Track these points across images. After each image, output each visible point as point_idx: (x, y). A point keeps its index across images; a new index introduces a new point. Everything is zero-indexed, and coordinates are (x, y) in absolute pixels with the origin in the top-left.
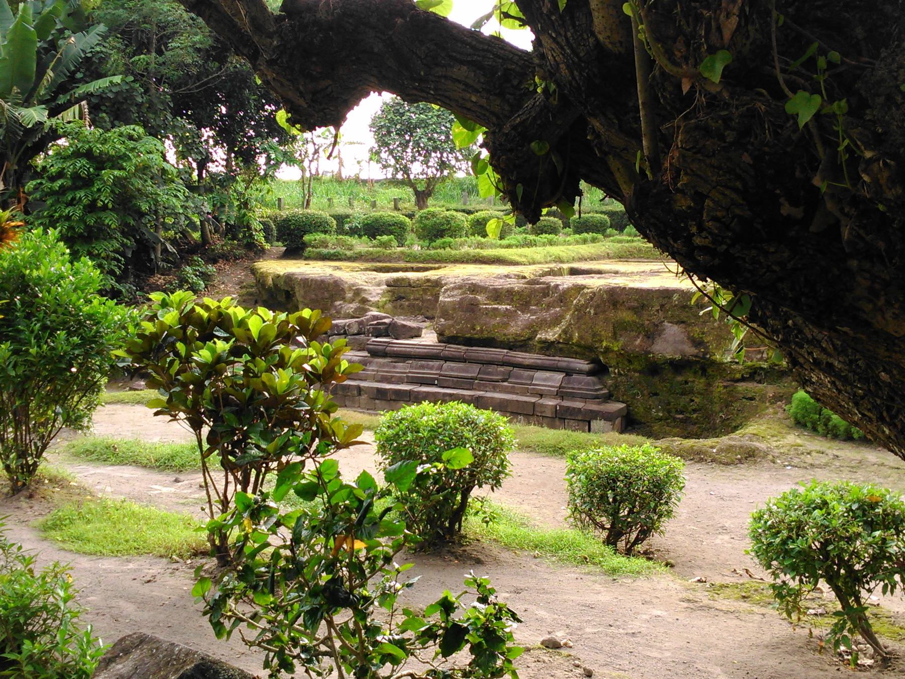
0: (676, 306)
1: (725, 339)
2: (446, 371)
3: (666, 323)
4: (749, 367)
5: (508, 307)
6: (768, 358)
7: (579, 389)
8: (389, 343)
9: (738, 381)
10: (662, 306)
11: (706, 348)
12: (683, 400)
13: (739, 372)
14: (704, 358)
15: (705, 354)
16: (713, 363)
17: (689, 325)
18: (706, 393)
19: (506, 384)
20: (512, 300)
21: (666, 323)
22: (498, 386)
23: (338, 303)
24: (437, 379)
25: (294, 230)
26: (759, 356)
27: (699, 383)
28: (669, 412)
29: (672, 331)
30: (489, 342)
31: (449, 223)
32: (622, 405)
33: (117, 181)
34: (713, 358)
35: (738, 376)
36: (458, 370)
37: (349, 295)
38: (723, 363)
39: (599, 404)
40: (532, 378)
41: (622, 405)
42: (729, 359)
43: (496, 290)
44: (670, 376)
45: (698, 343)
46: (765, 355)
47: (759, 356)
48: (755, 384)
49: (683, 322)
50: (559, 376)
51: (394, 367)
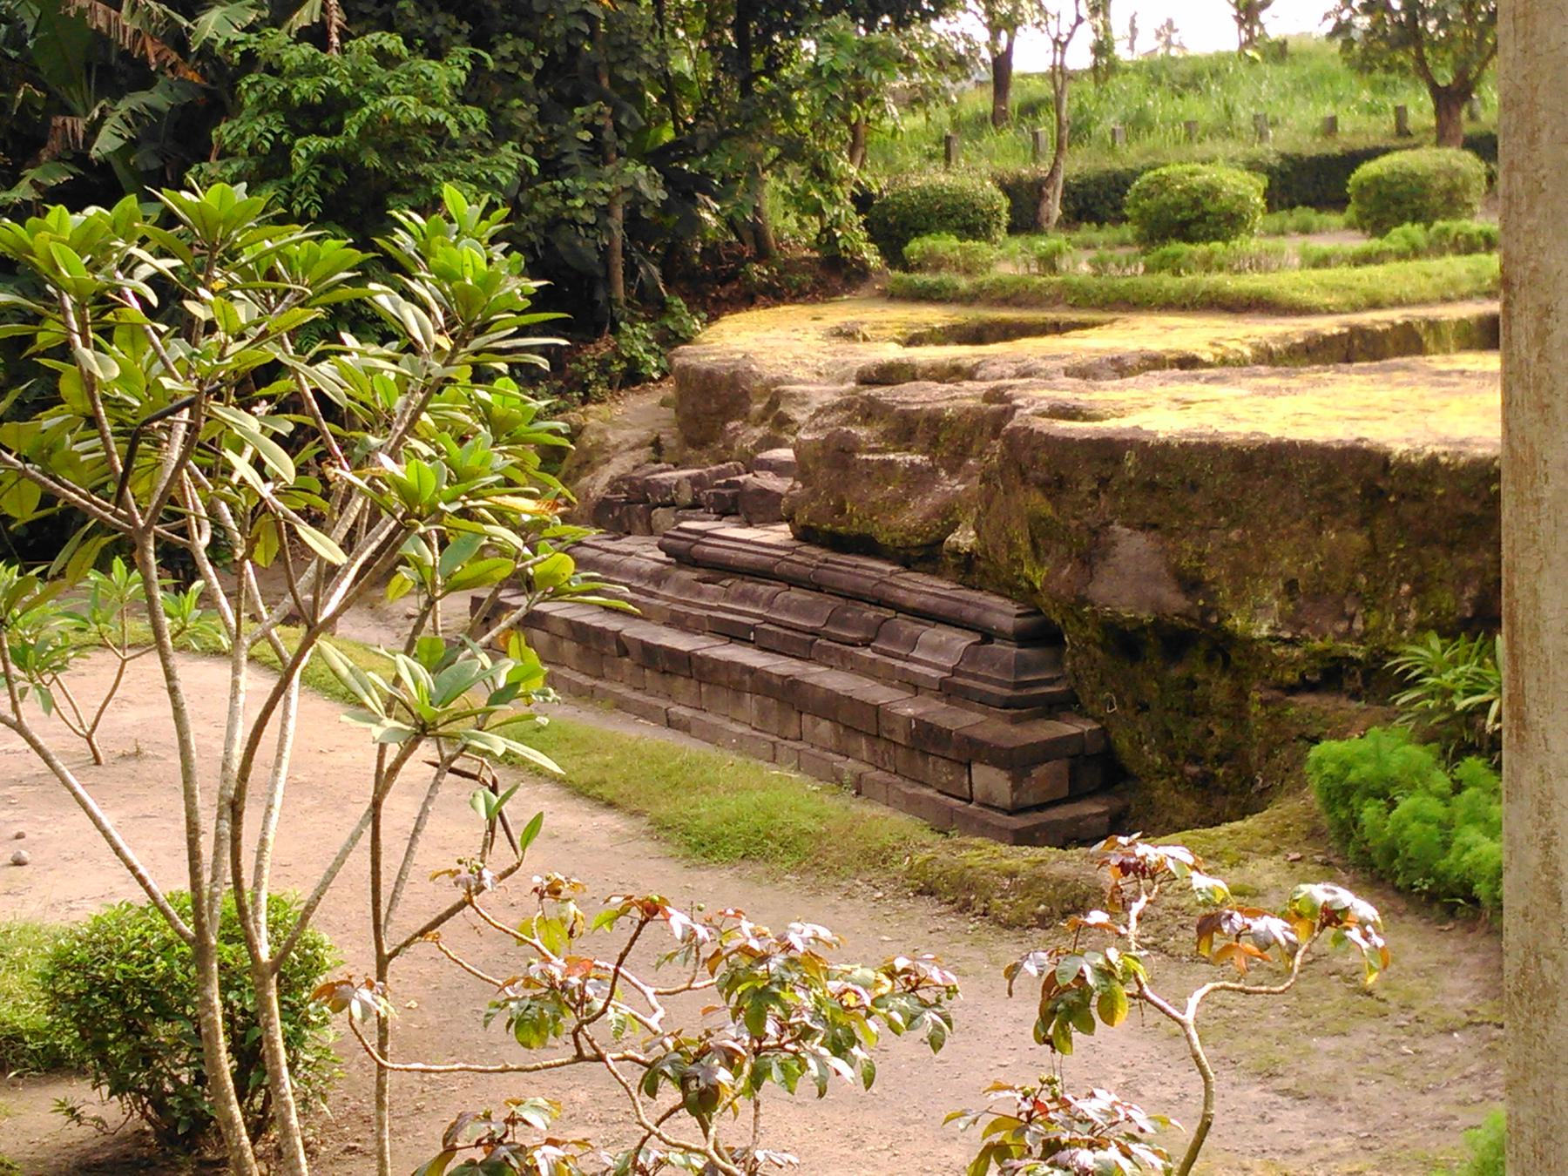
0: (1131, 482)
1: (1255, 576)
2: (777, 610)
3: (1117, 527)
4: (1315, 655)
5: (918, 459)
6: (1366, 634)
7: (988, 680)
8: (704, 534)
9: (1292, 690)
10: (1103, 482)
11: (1210, 596)
12: (1195, 728)
13: (1294, 664)
14: (1204, 623)
15: (1206, 612)
16: (1230, 638)
17: (1171, 532)
18: (1237, 715)
19: (868, 653)
20: (935, 442)
21: (1117, 527)
22: (844, 657)
23: (731, 425)
24: (753, 628)
25: (894, 226)
26: (1342, 627)
27: (1219, 690)
28: (1173, 756)
29: (1131, 545)
30: (867, 546)
31: (1196, 203)
32: (1087, 726)
33: (325, 160)
34: (1229, 623)
35: (1290, 677)
36: (802, 610)
37: (757, 407)
38: (1253, 640)
39: (1015, 721)
40: (913, 642)
41: (1087, 726)
42: (1265, 632)
43: (905, 415)
44: (1157, 663)
45: (1190, 584)
46: (1358, 625)
47: (1342, 627)
48: (1343, 702)
49: (1155, 526)
50: (961, 641)
51: (700, 594)
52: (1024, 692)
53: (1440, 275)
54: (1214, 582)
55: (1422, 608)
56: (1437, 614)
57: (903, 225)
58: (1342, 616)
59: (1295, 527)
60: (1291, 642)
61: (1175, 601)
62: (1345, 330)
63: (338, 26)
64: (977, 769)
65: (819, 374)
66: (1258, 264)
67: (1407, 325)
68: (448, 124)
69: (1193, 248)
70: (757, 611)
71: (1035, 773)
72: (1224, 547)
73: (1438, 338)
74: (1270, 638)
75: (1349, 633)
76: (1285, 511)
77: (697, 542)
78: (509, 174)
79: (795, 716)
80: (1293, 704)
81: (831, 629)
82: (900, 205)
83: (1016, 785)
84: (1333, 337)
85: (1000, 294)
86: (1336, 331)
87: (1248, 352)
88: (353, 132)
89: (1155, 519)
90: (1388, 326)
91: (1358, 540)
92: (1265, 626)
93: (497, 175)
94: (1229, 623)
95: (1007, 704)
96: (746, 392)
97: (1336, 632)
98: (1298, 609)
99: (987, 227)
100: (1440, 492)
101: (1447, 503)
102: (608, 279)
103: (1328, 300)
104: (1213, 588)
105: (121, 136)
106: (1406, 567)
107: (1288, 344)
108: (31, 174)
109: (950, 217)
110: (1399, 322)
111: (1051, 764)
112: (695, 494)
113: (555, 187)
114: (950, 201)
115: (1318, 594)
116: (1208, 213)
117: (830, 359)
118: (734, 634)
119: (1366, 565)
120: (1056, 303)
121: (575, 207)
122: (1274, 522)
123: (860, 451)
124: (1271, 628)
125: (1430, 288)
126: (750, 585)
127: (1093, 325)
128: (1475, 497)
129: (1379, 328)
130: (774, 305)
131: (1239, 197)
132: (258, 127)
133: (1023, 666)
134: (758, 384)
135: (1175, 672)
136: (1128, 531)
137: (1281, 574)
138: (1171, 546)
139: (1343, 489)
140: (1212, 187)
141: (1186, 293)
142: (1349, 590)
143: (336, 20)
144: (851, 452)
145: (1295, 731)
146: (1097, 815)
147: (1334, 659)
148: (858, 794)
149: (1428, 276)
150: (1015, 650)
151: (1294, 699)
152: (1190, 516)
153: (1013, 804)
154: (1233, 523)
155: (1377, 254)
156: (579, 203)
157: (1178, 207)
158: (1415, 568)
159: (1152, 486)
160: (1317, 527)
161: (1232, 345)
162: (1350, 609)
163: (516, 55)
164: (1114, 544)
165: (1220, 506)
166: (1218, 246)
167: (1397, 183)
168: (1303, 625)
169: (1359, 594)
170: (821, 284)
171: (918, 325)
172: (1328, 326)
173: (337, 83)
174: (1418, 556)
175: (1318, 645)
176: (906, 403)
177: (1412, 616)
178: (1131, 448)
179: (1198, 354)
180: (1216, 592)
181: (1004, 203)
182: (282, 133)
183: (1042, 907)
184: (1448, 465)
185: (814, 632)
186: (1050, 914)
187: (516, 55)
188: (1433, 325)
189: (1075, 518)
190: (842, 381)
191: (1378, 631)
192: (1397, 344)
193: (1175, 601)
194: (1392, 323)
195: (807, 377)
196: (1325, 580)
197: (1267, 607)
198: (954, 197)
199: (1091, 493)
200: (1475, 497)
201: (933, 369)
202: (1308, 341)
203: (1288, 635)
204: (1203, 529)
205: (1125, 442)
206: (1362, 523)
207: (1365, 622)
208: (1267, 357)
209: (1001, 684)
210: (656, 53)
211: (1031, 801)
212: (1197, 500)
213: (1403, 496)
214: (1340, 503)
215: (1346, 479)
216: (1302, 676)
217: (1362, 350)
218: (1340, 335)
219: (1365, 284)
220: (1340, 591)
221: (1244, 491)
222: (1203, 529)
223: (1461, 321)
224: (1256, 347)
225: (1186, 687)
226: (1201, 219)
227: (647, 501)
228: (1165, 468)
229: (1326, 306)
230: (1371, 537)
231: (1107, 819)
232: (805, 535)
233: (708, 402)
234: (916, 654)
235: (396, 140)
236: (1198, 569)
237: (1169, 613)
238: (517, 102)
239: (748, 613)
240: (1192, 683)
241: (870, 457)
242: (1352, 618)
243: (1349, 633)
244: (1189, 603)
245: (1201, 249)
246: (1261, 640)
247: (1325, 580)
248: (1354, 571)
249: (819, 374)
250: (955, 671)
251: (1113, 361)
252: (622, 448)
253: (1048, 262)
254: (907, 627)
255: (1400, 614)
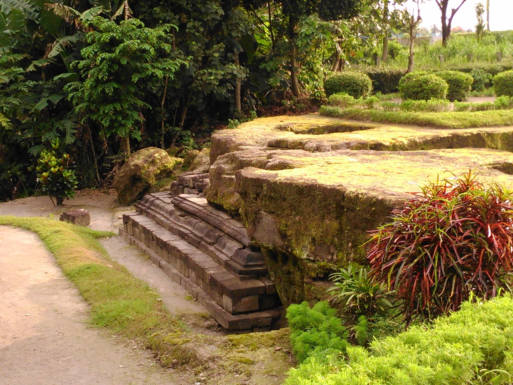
1: (303, 235)
4: (320, 267)
6: (337, 261)
10: (258, 195)
13: (314, 270)
15: (288, 247)
17: (278, 215)
21: (263, 212)
26: (330, 257)
31: (421, 86)
34: (294, 252)
35: (313, 274)
39: (242, 279)
45: (284, 236)
47: (330, 257)
51: (179, 220)
52: (248, 269)
53: (506, 116)
54: (290, 236)
55: (355, 252)
56: (360, 256)
57: (332, 89)
58: (329, 253)
59: (316, 217)
60: (313, 261)
61: (279, 242)
62: (450, 135)
63: (128, 16)
64: (224, 296)
65: (257, 142)
66: (433, 109)
67: (478, 134)
68: (151, 50)
69: (414, 102)
70: (190, 229)
71: (243, 300)
72: (294, 223)
73: (493, 140)
74: (307, 259)
75: (331, 260)
76: (313, 211)
77: (181, 202)
78: (177, 68)
79: (187, 268)
80: (314, 285)
81: (206, 238)
82: (331, 82)
83: (234, 303)
84: (444, 138)
85: (351, 115)
86: (446, 136)
87: (406, 142)
88: (117, 51)
89: (272, 210)
90: (470, 135)
91: (335, 224)
92: (306, 254)
93: (172, 68)
94: (294, 252)
95: (241, 273)
96: (228, 148)
97: (328, 259)
98: (316, 249)
99: (362, 91)
100: (358, 208)
101: (360, 213)
102: (235, 104)
103: (454, 124)
104: (290, 238)
105: (58, 51)
106: (350, 237)
107: (424, 140)
108: (35, 62)
109: (347, 87)
110: (475, 133)
111: (251, 297)
112: (194, 184)
113: (204, 72)
114: (347, 81)
115: (322, 244)
116: (425, 89)
117: (263, 137)
118: (183, 236)
119: (337, 234)
120: (367, 119)
121: (211, 79)
122: (309, 214)
123: (224, 174)
124: (307, 255)
125: (500, 120)
126: (192, 219)
127: (369, 128)
128: (368, 212)
129: (465, 135)
130: (292, 115)
131: (437, 84)
132: (90, 49)
133: (250, 258)
134: (234, 145)
135: (285, 268)
136: (266, 213)
137: (311, 235)
138: (278, 221)
139: (330, 204)
140: (427, 80)
141: (406, 119)
142: (332, 243)
143: (127, 14)
144: (221, 174)
145: (314, 296)
146: (268, 317)
147: (327, 269)
148: (197, 300)
149: (501, 116)
150: (250, 252)
151: (315, 283)
152: (284, 210)
153: (233, 311)
154: (297, 215)
155: (487, 106)
156: (212, 78)
157: (413, 87)
158: (353, 237)
159: (271, 198)
160: (323, 218)
161: (400, 139)
162: (332, 251)
163: (194, 27)
164: (262, 218)
165: (293, 208)
166: (423, 102)
167: (508, 81)
168: (317, 255)
169: (335, 245)
170: (310, 108)
171: (314, 125)
172: (445, 133)
173: (115, 35)
174: (354, 232)
175: (322, 264)
176: (243, 157)
177: (352, 255)
178: (265, 183)
179: (383, 143)
180: (291, 240)
181: (370, 82)
182: (98, 51)
183: (175, 360)
184: (361, 198)
185: (201, 238)
186: (177, 364)
187: (194, 27)
188: (490, 135)
189: (251, 207)
190: (263, 146)
191: (341, 260)
192: (473, 141)
193: (279, 242)
194: (472, 134)
195: (252, 143)
196: (324, 239)
197: (306, 247)
198: (350, 80)
199: (254, 198)
200: (368, 212)
201: (293, 143)
202: (432, 139)
203: (312, 259)
204: (288, 215)
205: (263, 180)
206: (337, 218)
207: (337, 256)
208: (414, 145)
209: (241, 265)
210: (244, 27)
211: (241, 310)
212: (285, 204)
213: (348, 209)
214: (329, 209)
215: (330, 200)
216: (317, 274)
217: (457, 143)
218: (448, 137)
219: (472, 118)
220: (329, 244)
221: (300, 202)
222: (288, 215)
223: (504, 134)
224: (410, 141)
225: (288, 274)
226: (422, 91)
227: (183, 185)
228: (275, 191)
229: (453, 126)
230: (340, 224)
231: (270, 319)
232: (210, 203)
233: (217, 150)
234: (223, 251)
235: (67, 55)
236: (286, 230)
237: (278, 246)
238: (194, 43)
239: (187, 229)
240: (289, 273)
241: (226, 176)
242: (333, 255)
243: (331, 260)
244: (283, 243)
245: (417, 102)
246: (304, 259)
247: (324, 239)
248: (333, 236)
249: (257, 142)
250: (231, 259)
251: (347, 144)
252: (206, 163)
253: (370, 104)
254: (225, 239)
255: (348, 254)
